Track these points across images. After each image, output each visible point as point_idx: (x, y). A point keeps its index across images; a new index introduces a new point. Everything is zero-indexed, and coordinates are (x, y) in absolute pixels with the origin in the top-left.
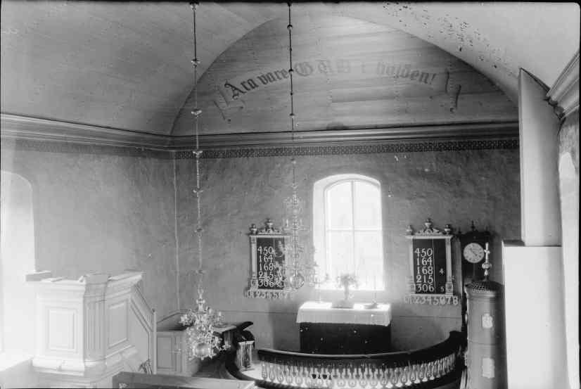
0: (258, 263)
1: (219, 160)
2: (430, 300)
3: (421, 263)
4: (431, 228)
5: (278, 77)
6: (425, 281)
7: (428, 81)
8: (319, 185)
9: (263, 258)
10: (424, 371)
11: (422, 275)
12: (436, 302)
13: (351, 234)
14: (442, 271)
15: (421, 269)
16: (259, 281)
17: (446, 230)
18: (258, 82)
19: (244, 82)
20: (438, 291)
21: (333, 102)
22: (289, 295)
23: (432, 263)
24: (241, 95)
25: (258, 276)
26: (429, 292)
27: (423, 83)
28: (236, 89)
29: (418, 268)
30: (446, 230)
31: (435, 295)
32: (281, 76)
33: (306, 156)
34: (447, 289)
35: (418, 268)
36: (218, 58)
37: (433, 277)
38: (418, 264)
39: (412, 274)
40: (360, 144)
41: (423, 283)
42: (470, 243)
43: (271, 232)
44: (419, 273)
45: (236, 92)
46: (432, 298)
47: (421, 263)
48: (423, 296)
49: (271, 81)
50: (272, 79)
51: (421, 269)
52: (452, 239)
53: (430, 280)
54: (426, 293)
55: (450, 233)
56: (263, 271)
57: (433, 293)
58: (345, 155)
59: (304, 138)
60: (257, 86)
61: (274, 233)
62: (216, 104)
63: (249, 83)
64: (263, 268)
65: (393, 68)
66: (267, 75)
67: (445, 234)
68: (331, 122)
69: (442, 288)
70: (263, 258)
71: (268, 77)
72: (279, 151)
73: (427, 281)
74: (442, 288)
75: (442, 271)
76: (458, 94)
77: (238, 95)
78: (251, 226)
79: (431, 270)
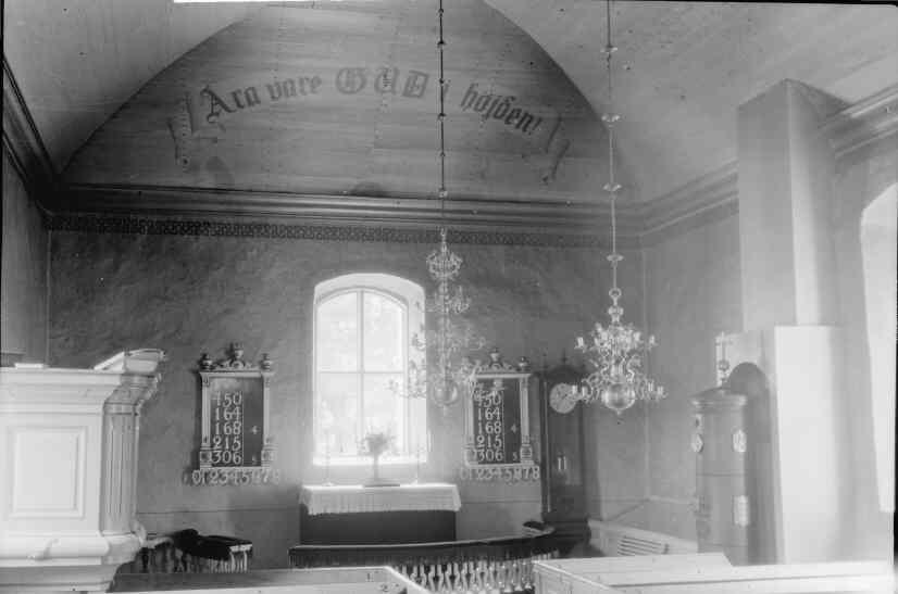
0: (213, 422)
1: (141, 238)
2: (500, 473)
3: (483, 417)
4: (500, 362)
5: (302, 91)
6: (227, 447)
7: (528, 129)
8: (321, 288)
9: (483, 411)
10: (517, 575)
11: (486, 436)
12: (508, 475)
13: (367, 367)
14: (514, 428)
15: (483, 426)
16: (214, 455)
17: (521, 365)
18: (264, 95)
19: (239, 91)
20: (509, 460)
21: (377, 145)
22: (270, 477)
23: (501, 416)
24: (225, 116)
25: (212, 445)
26: (495, 462)
27: (520, 131)
28: (219, 102)
29: (218, 425)
30: (521, 365)
31: (244, 469)
32: (307, 88)
33: (301, 241)
34: (522, 456)
35: (218, 425)
36: (208, 40)
37: (501, 438)
38: (480, 418)
39: (472, 434)
40: (397, 225)
41: (486, 448)
42: (559, 383)
43: (241, 367)
44: (480, 432)
45: (217, 108)
46: (503, 470)
47: (483, 417)
48: (487, 466)
49: (287, 96)
50: (290, 92)
51: (483, 426)
52: (530, 378)
53: (236, 445)
54: (493, 463)
55: (527, 370)
56: (222, 435)
57: (502, 462)
58: (368, 242)
59: (480, 212)
60: (258, 102)
61: (245, 369)
62: (170, 126)
63: (484, 108)
64: (484, 430)
65: (489, 98)
66: (285, 83)
67: (519, 370)
68: (363, 180)
69: (515, 454)
70: (483, 411)
71: (285, 88)
72: (259, 229)
73: (230, 446)
74: (515, 454)
75: (514, 428)
76: (560, 156)
77: (217, 114)
78: (200, 357)
79: (498, 428)
